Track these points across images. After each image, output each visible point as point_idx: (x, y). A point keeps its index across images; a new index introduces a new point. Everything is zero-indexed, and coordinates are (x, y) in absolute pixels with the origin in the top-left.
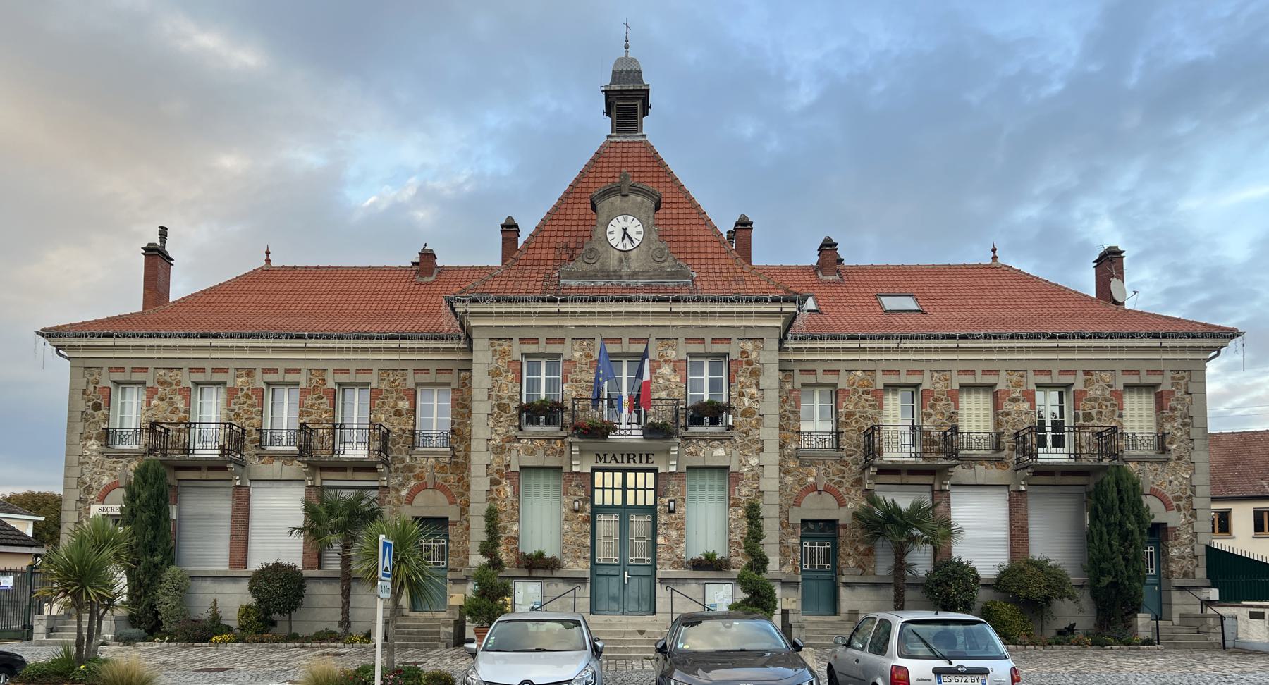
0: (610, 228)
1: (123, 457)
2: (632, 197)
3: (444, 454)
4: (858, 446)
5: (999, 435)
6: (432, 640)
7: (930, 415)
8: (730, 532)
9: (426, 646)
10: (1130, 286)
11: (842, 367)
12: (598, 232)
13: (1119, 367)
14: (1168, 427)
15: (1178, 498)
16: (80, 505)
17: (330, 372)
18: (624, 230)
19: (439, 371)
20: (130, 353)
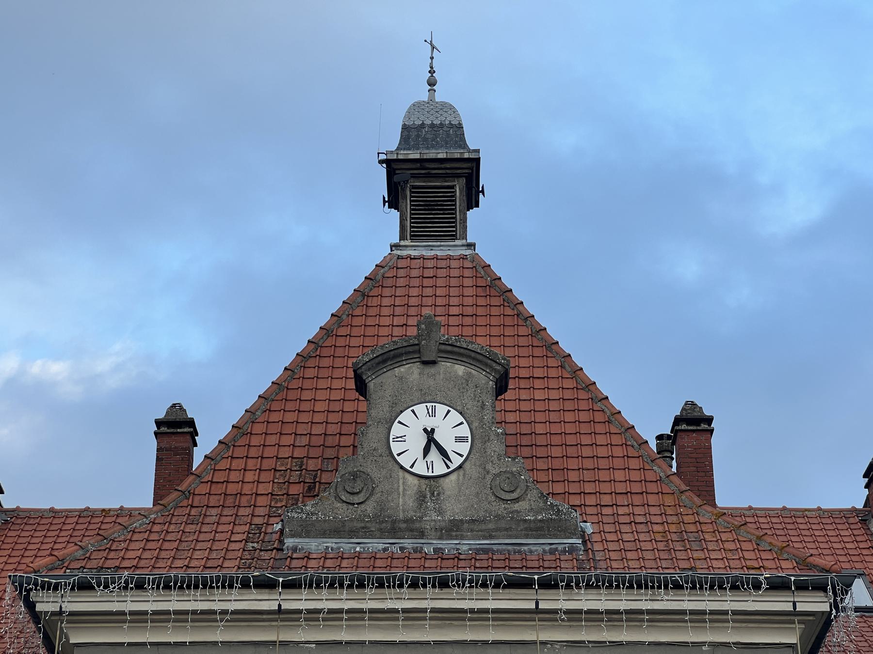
0: (396, 430)
12: (373, 436)
18: (430, 433)
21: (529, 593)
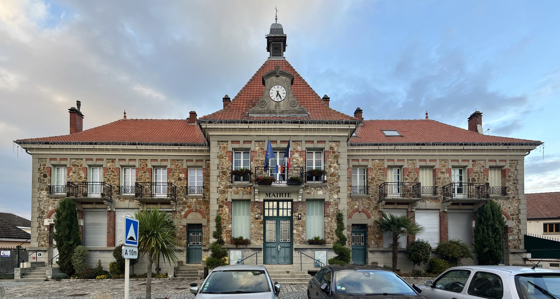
0: (271, 91)
1: (58, 198)
2: (281, 77)
3: (200, 197)
4: (376, 192)
5: (436, 187)
6: (195, 276)
7: (407, 179)
8: (325, 228)
9: (192, 279)
10: (486, 125)
11: (370, 158)
12: (266, 93)
13: (487, 158)
14: (507, 185)
15: (513, 215)
16: (39, 219)
17: (149, 161)
18: (278, 92)
19: (197, 161)
20: (58, 152)
21: (298, 125)
